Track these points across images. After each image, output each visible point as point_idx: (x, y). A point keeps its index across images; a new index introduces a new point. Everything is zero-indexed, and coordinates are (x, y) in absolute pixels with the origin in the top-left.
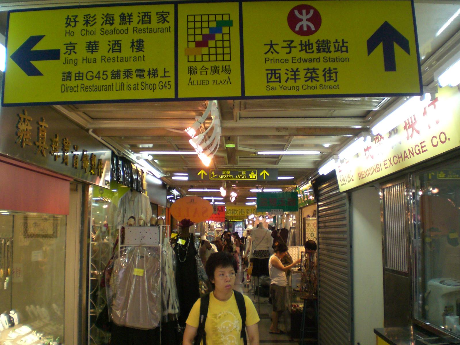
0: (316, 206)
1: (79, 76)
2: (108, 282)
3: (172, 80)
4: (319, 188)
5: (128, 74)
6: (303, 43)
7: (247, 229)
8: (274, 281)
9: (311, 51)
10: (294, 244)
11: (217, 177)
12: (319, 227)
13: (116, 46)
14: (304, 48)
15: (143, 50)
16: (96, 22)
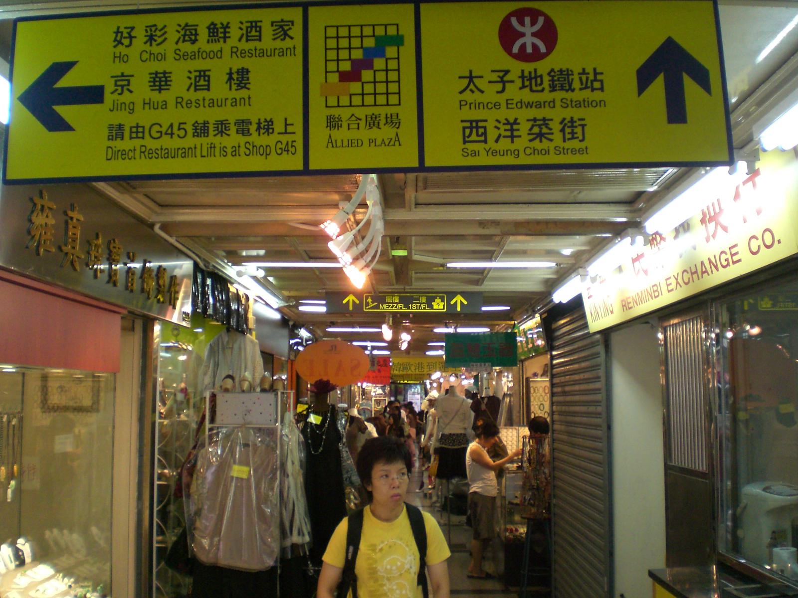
0: (549, 356)
1: (138, 131)
2: (187, 490)
3: (299, 138)
4: (554, 326)
5: (222, 127)
6: (526, 74)
7: (428, 397)
8: (475, 488)
9: (540, 88)
10: (510, 423)
11: (377, 307)
12: (553, 394)
13: (202, 80)
14: (527, 83)
15: (248, 86)
16: (166, 39)
